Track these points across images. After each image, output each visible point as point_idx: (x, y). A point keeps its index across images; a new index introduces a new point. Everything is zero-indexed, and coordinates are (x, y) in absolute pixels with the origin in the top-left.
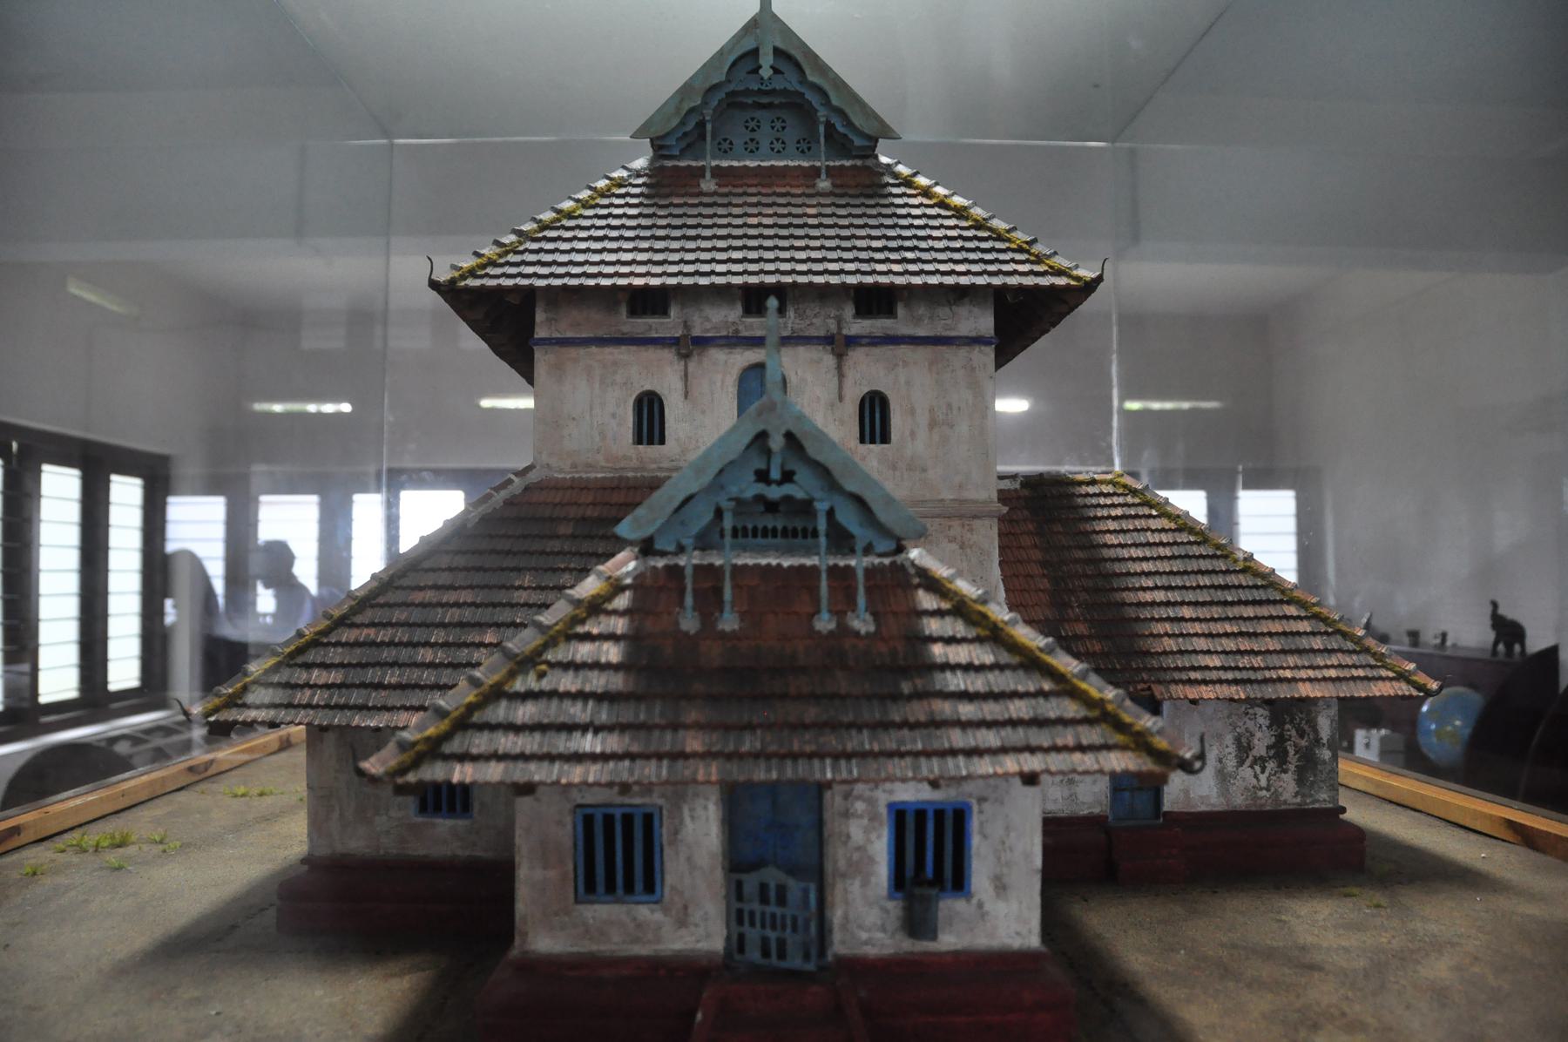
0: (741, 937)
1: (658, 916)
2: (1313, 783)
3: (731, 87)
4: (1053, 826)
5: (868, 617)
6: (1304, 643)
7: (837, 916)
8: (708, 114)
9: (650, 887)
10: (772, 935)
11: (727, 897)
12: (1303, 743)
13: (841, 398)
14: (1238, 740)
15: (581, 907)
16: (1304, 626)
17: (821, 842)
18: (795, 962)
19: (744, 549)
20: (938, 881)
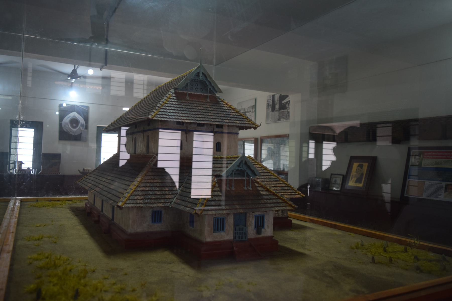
4: (275, 219)
6: (284, 188)
9: (223, 229)
10: (241, 235)
16: (284, 185)
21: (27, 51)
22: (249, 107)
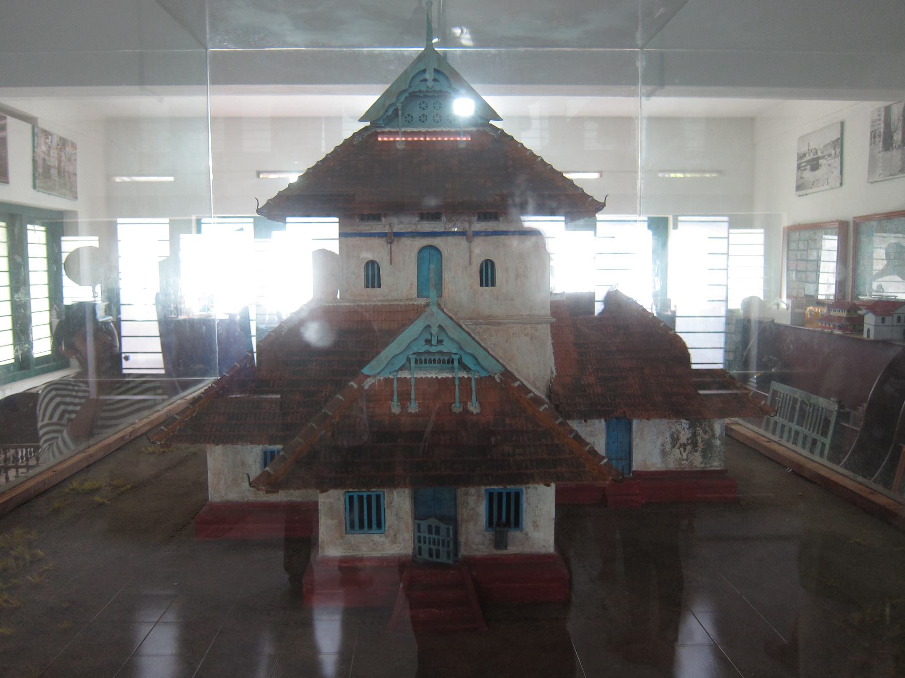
0: (420, 548)
1: (383, 539)
2: (710, 458)
3: (411, 91)
5: (477, 405)
7: (462, 539)
8: (399, 106)
9: (379, 526)
11: (414, 531)
12: (706, 437)
13: (470, 264)
14: (672, 436)
15: (349, 536)
17: (455, 506)
18: (443, 559)
19: (421, 369)
20: (508, 524)
21: (214, 82)
22: (825, 146)
